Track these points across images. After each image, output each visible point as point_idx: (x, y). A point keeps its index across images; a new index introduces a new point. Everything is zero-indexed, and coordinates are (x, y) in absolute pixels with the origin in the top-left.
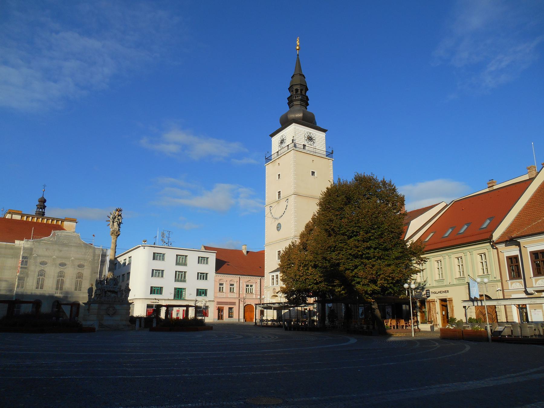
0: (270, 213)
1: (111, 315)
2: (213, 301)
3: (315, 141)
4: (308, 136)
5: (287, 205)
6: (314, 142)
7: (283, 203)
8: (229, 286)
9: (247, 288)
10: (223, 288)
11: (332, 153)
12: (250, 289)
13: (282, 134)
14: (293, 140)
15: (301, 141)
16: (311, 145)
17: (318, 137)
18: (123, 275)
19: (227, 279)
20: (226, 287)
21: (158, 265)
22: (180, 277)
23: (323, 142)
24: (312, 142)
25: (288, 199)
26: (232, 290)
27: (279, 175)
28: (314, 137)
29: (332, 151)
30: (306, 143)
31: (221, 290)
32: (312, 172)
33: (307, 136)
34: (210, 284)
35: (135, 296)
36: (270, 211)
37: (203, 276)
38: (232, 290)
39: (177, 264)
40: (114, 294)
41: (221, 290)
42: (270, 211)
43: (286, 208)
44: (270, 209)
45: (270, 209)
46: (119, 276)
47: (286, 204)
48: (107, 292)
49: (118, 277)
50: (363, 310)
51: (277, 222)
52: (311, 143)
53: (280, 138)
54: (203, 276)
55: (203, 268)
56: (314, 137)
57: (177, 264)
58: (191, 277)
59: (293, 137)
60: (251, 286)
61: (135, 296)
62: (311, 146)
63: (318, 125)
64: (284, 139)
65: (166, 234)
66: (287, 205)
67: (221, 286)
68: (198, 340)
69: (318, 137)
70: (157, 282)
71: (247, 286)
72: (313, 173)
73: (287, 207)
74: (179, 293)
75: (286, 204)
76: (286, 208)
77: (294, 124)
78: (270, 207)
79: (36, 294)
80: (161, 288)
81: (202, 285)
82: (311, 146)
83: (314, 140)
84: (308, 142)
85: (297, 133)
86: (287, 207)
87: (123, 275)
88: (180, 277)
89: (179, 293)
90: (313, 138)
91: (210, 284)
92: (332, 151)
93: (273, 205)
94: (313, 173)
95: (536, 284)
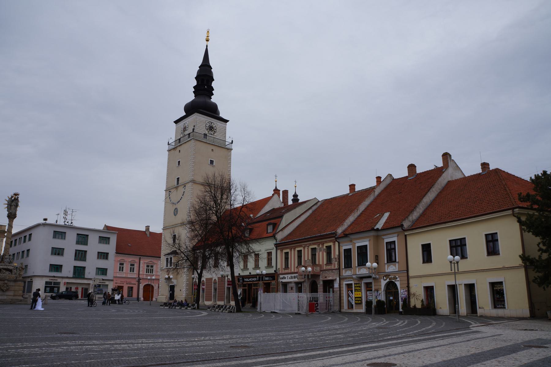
0: (169, 197)
1: (4, 291)
2: (112, 280)
3: (216, 131)
4: (209, 125)
5: (184, 192)
6: (215, 132)
7: (181, 189)
8: (129, 266)
9: (148, 268)
10: (153, 269)
11: (232, 143)
12: (151, 269)
13: (184, 122)
14: (193, 129)
15: (202, 129)
16: (211, 134)
17: (219, 127)
18: (23, 252)
19: (128, 260)
20: (127, 267)
21: (59, 243)
22: (81, 255)
23: (222, 134)
24: (213, 132)
25: (185, 186)
26: (132, 270)
27: (179, 162)
28: (215, 127)
29: (232, 141)
30: (207, 132)
31: (121, 269)
32: (210, 160)
33: (208, 126)
34: (111, 264)
35: (33, 273)
36: (169, 195)
37: (103, 256)
38: (132, 270)
39: (78, 243)
40: (8, 272)
41: (121, 269)
42: (169, 195)
43: (183, 194)
44: (169, 194)
45: (169, 194)
46: (19, 252)
47: (183, 190)
48: (2, 270)
49: (14, 254)
50: (241, 292)
51: (175, 207)
52: (212, 132)
53: (183, 126)
54: (103, 256)
55: (104, 248)
56: (215, 127)
57: (78, 243)
58: (92, 256)
59: (194, 126)
60: (152, 267)
61: (33, 273)
62: (212, 136)
63: (221, 115)
64: (187, 127)
65: (69, 212)
66: (184, 192)
67: (132, 267)
68: (307, 349)
69: (219, 127)
70: (56, 260)
71: (148, 266)
72: (212, 162)
73: (184, 193)
74: (79, 272)
75: (183, 190)
76: (183, 194)
77: (196, 114)
78: (169, 192)
79: (486, 315)
80: (61, 266)
81: (102, 264)
82: (212, 136)
83: (215, 129)
84: (209, 132)
85: (198, 123)
86: (184, 193)
87: (23, 252)
88: (81, 255)
89: (79, 272)
90: (215, 128)
91: (111, 264)
92: (232, 141)
93: (172, 191)
94: (212, 162)
95: (387, 270)
